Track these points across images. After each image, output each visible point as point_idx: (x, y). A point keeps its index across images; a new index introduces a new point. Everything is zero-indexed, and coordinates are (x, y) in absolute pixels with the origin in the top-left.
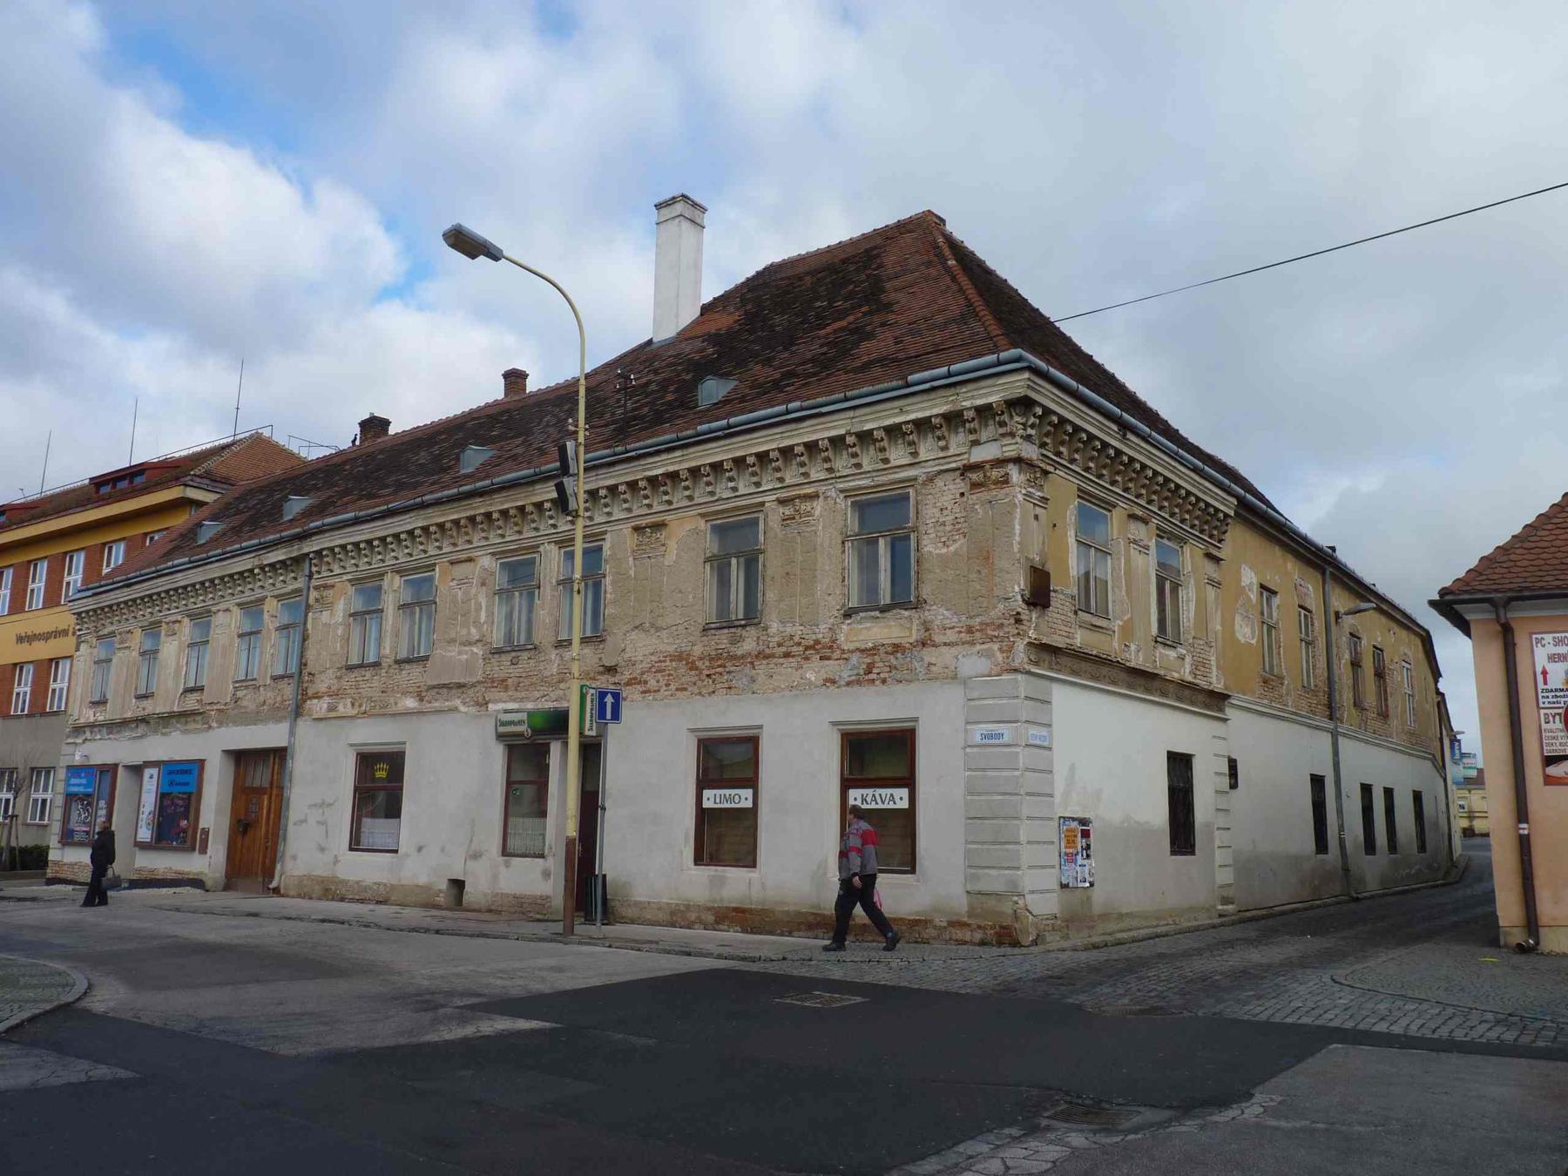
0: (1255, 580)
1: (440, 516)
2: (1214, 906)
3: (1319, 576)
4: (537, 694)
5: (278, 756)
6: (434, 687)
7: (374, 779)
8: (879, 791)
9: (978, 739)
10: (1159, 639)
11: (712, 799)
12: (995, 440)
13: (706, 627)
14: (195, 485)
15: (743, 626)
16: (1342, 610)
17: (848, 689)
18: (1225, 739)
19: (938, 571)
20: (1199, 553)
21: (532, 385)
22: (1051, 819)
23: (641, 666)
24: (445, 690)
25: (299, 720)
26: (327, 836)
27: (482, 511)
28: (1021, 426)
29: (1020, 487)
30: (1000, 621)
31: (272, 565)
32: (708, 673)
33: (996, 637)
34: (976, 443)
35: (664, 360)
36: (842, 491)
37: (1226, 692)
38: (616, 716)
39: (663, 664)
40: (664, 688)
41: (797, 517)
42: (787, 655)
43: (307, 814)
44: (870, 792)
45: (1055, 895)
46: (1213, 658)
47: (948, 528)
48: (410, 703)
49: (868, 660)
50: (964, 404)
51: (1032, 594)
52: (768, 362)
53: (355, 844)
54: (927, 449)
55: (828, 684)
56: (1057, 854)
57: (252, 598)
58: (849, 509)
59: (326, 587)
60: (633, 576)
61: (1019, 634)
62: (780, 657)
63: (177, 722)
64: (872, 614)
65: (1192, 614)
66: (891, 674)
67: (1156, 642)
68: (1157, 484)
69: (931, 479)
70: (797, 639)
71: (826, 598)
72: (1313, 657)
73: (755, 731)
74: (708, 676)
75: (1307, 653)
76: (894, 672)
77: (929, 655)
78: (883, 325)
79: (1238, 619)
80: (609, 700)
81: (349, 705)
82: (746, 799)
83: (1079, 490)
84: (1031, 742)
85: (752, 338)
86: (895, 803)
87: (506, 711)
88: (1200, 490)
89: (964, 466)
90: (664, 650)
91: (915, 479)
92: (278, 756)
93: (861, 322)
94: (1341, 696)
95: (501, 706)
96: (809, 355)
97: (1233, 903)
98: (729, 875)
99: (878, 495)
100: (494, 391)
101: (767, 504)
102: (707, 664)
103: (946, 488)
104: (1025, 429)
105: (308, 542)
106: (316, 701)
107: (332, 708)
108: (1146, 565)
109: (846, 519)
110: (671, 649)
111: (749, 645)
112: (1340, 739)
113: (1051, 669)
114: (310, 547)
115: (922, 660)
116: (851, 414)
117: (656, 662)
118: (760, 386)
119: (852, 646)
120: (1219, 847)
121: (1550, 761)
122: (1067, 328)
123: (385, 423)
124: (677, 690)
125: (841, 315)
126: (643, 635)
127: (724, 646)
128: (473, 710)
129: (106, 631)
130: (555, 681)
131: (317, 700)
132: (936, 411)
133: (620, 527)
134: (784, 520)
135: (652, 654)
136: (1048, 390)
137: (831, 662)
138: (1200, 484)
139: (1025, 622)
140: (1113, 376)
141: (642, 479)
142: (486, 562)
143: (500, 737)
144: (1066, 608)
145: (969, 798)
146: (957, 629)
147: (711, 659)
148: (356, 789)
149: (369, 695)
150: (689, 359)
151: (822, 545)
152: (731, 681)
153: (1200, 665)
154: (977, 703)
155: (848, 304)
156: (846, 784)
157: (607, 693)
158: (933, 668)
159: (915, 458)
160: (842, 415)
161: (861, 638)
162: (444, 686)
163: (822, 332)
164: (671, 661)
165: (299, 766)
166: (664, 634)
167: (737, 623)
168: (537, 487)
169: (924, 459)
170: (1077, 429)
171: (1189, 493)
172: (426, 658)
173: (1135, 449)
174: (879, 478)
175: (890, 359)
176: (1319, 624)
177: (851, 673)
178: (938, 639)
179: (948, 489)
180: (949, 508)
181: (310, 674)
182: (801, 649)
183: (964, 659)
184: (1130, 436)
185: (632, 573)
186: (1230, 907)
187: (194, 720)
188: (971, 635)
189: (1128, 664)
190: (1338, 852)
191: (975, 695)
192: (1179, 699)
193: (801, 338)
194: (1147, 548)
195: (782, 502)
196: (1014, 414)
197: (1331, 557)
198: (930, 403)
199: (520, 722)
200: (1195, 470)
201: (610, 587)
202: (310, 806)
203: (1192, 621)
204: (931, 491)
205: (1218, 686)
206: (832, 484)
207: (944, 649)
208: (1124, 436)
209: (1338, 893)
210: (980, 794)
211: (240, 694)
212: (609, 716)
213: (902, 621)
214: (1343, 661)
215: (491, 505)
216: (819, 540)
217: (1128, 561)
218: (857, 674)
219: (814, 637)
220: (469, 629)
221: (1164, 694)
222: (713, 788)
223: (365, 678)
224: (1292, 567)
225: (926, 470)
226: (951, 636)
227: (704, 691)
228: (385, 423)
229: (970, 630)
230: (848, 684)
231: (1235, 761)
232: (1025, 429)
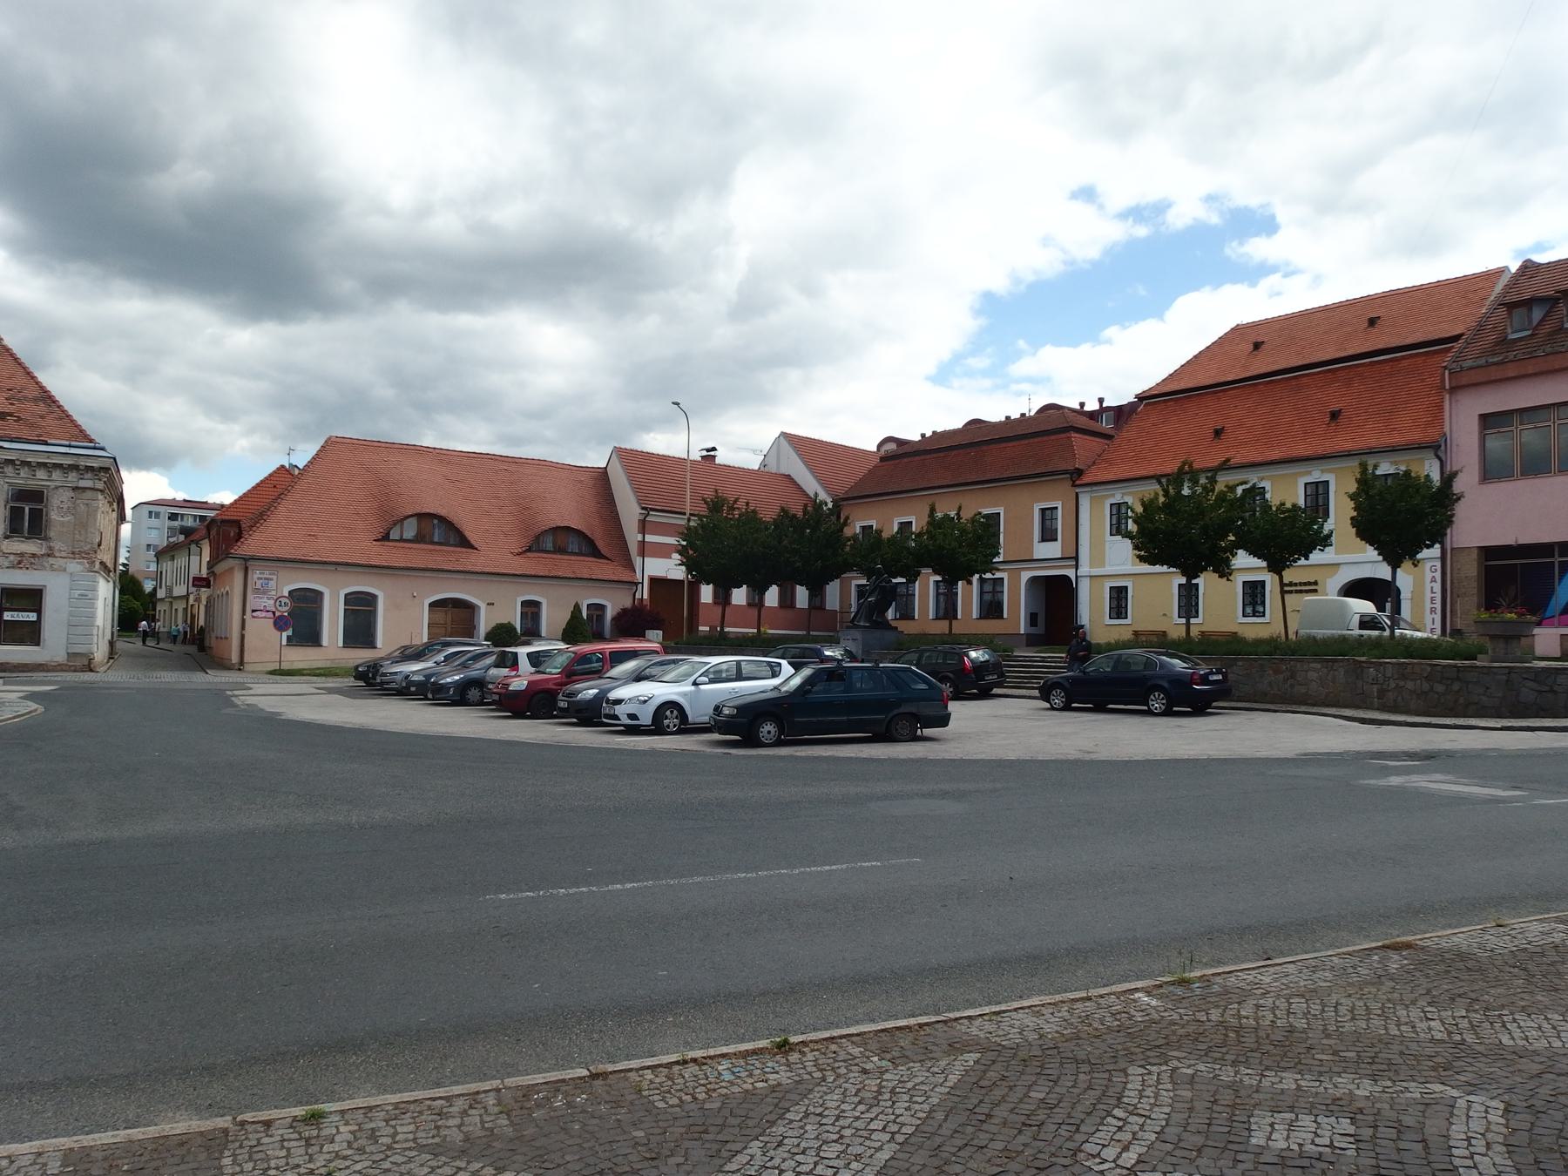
54: (56, 475)
77: (51, 560)
121: (253, 611)
226: (63, 554)
229: (73, 553)
230: (8, 568)
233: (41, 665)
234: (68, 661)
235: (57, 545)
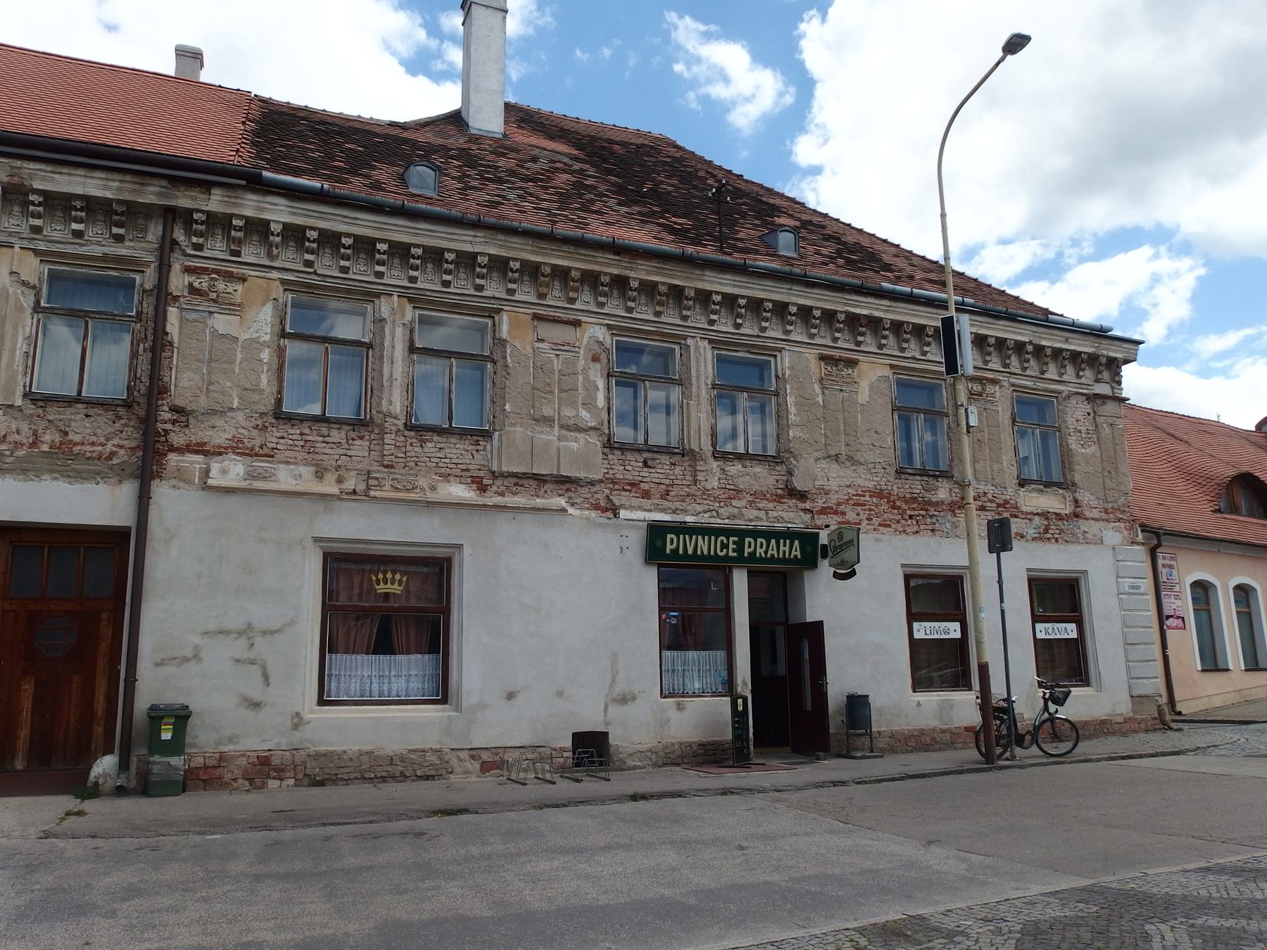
1: (533, 252)
4: (699, 508)
8: (1057, 625)
24: (534, 483)
25: (155, 484)
34: (1098, 381)
36: (1012, 385)
39: (862, 498)
40: (866, 522)
41: (984, 395)
48: (459, 491)
60: (821, 404)
74: (911, 517)
76: (1063, 534)
103: (1078, 406)
110: (870, 485)
116: (1034, 328)
124: (880, 525)
127: (918, 491)
133: (801, 350)
135: (849, 486)
151: (1003, 423)
152: (934, 524)
160: (1028, 327)
164: (870, 496)
166: (861, 469)
180: (1082, 421)
182: (994, 505)
198: (1083, 343)
201: (793, 408)
207: (1092, 522)
215: (631, 269)
220: (577, 410)
226: (1095, 513)
227: (909, 530)
229: (1106, 512)
230: (1033, 539)
233: (1103, 722)
234: (1134, 712)
235: (1085, 497)
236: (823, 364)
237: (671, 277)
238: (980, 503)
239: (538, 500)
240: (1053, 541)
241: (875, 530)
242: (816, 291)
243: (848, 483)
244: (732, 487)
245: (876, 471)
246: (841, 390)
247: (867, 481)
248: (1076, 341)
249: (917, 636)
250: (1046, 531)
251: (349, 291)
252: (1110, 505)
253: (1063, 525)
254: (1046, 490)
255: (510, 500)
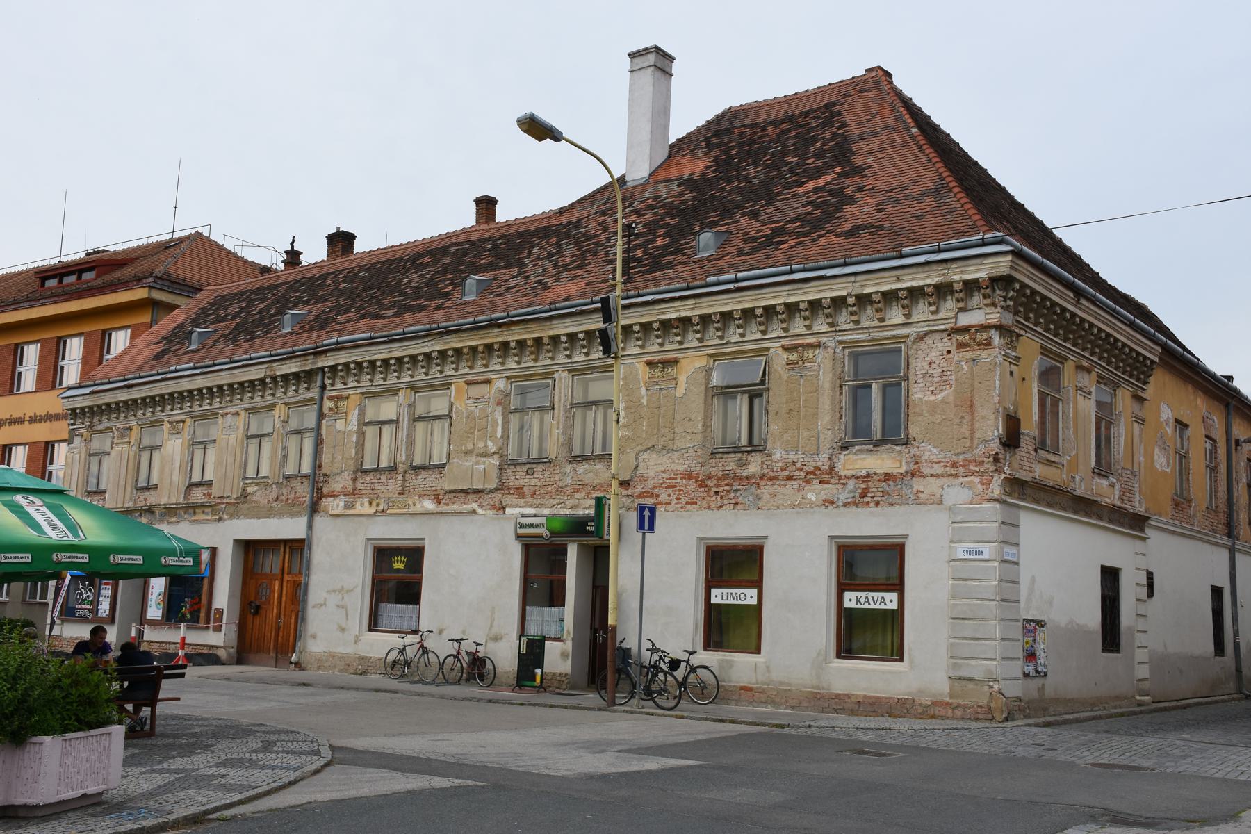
0: (1171, 416)
1: (457, 342)
2: (1134, 697)
3: (1222, 407)
5: (297, 548)
6: (451, 492)
7: (391, 569)
8: (871, 594)
9: (961, 555)
10: (1096, 470)
11: (720, 597)
12: (980, 308)
13: (715, 451)
14: (158, 286)
15: (749, 452)
16: (1242, 439)
17: (846, 509)
18: (1144, 555)
19: (926, 415)
20: (1128, 394)
21: (503, 214)
22: (1017, 621)
23: (652, 482)
24: (463, 495)
26: (347, 619)
27: (500, 339)
28: (1002, 299)
29: (1000, 348)
30: (981, 459)
31: (285, 377)
32: (717, 490)
33: (978, 472)
35: (643, 202)
36: (840, 343)
37: (1147, 515)
38: (652, 528)
39: (674, 481)
40: (676, 501)
41: (800, 363)
42: (789, 478)
43: (325, 599)
44: (863, 595)
45: (1020, 681)
46: (1137, 486)
47: (936, 379)
48: (429, 505)
49: (863, 486)
50: (954, 277)
51: (1007, 436)
52: (754, 215)
53: (374, 625)
54: (922, 312)
55: (827, 504)
56: (1021, 649)
57: (263, 404)
58: (847, 358)
59: (340, 398)
60: (645, 404)
61: (996, 470)
62: (783, 480)
63: (185, 513)
64: (867, 447)
65: (1122, 448)
66: (883, 498)
67: (1094, 473)
68: (1124, 353)
69: (921, 337)
70: (798, 465)
71: (826, 432)
72: (1216, 481)
73: (759, 541)
74: (717, 493)
75: (1210, 477)
77: (918, 484)
78: (861, 189)
79: (1157, 451)
80: (647, 513)
81: (367, 504)
82: (751, 597)
83: (1041, 347)
84: (1006, 558)
85: (729, 187)
86: (885, 604)
87: (523, 516)
88: (1133, 342)
89: (952, 329)
90: (675, 469)
91: (907, 336)
92: (297, 548)
93: (839, 184)
94: (1238, 515)
95: (518, 511)
96: (795, 214)
97: (1148, 695)
98: (735, 659)
99: (872, 348)
100: (466, 218)
101: (772, 350)
102: (715, 482)
104: (1005, 301)
105: (323, 358)
106: (331, 499)
107: (348, 506)
108: (1088, 407)
109: (844, 367)
110: (682, 468)
111: (754, 468)
112: (1237, 554)
113: (1019, 499)
114: (323, 362)
115: (912, 487)
116: (852, 279)
117: (667, 479)
118: (754, 239)
119: (849, 473)
120: (1139, 647)
122: (1057, 233)
123: (351, 237)
124: (687, 503)
125: (817, 174)
126: (654, 456)
127: (730, 468)
128: (490, 513)
129: (101, 427)
130: (570, 491)
131: (332, 499)
132: (929, 282)
134: (788, 364)
135: (664, 472)
136: (1024, 268)
137: (830, 485)
138: (1133, 336)
139: (1002, 461)
140: (1004, 190)
141: (656, 322)
142: (500, 384)
143: (518, 537)
144: (1030, 447)
145: (952, 602)
146: (942, 464)
147: (719, 479)
148: (373, 580)
149: (387, 496)
150: (668, 203)
153: (1126, 492)
154: (960, 525)
155: (819, 163)
156: (842, 589)
157: (645, 508)
158: (921, 495)
159: (908, 318)
161: (856, 467)
162: (462, 491)
163: (800, 190)
164: (681, 478)
165: (319, 556)
166: (675, 455)
167: (743, 449)
168: (554, 322)
169: (916, 320)
170: (1044, 298)
171: (1124, 345)
172: (443, 466)
173: (1086, 312)
174: (875, 334)
175: (876, 227)
176: (1222, 451)
177: (848, 496)
178: (926, 470)
179: (937, 347)
180: (937, 362)
181: (325, 475)
182: (802, 473)
183: (948, 489)
184: (1083, 302)
185: (644, 401)
186: (1147, 698)
187: (203, 512)
188: (955, 469)
189: (1075, 493)
190: (1233, 656)
191: (959, 519)
192: (1111, 522)
193: (780, 193)
194: (1089, 393)
195: (787, 349)
196: (996, 288)
197: (1227, 386)
198: (923, 275)
199: (539, 526)
200: (1132, 325)
202: (329, 592)
203: (1122, 454)
204: (921, 347)
205: (1141, 510)
206: (832, 336)
208: (1078, 301)
209: (1232, 692)
210: (961, 599)
211: (250, 490)
212: (646, 527)
213: (893, 455)
214: (1241, 484)
215: (509, 335)
216: (820, 383)
217: (1076, 408)
218: (853, 497)
219: (814, 464)
220: (486, 443)
221: (1100, 518)
222: (721, 587)
223: (380, 481)
224: (1201, 404)
225: (918, 330)
226: (938, 469)
227: (713, 505)
228: (351, 237)
229: (954, 465)
230: (845, 505)
231: (1152, 573)
232: (1005, 301)
235: (928, 451)
236: (648, 369)
237: (533, 332)
238: (787, 473)
239: (464, 506)
240: (872, 505)
241: (682, 508)
242: (631, 311)
243: (663, 469)
244: (580, 483)
245: (688, 455)
246: (661, 389)
247: (678, 464)
248: (910, 277)
249: (714, 601)
250: (864, 495)
251: (388, 391)
252: (962, 457)
253: (890, 487)
254: (875, 449)
255: (454, 507)
